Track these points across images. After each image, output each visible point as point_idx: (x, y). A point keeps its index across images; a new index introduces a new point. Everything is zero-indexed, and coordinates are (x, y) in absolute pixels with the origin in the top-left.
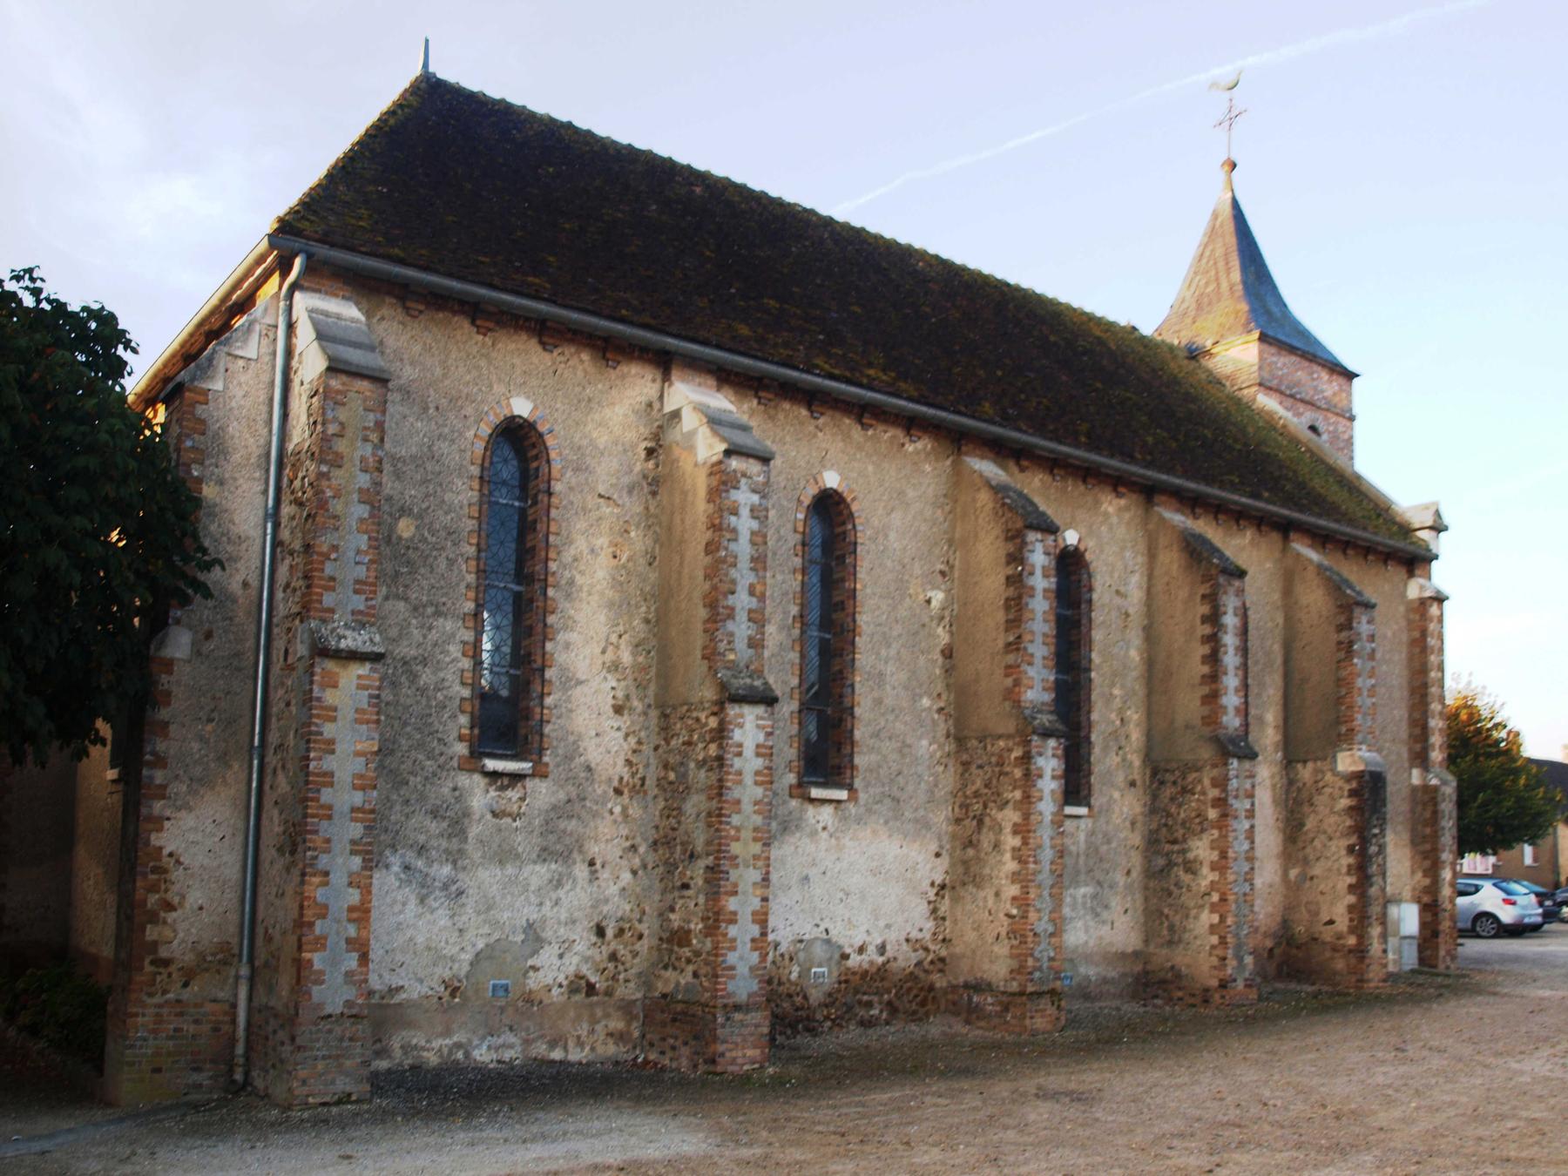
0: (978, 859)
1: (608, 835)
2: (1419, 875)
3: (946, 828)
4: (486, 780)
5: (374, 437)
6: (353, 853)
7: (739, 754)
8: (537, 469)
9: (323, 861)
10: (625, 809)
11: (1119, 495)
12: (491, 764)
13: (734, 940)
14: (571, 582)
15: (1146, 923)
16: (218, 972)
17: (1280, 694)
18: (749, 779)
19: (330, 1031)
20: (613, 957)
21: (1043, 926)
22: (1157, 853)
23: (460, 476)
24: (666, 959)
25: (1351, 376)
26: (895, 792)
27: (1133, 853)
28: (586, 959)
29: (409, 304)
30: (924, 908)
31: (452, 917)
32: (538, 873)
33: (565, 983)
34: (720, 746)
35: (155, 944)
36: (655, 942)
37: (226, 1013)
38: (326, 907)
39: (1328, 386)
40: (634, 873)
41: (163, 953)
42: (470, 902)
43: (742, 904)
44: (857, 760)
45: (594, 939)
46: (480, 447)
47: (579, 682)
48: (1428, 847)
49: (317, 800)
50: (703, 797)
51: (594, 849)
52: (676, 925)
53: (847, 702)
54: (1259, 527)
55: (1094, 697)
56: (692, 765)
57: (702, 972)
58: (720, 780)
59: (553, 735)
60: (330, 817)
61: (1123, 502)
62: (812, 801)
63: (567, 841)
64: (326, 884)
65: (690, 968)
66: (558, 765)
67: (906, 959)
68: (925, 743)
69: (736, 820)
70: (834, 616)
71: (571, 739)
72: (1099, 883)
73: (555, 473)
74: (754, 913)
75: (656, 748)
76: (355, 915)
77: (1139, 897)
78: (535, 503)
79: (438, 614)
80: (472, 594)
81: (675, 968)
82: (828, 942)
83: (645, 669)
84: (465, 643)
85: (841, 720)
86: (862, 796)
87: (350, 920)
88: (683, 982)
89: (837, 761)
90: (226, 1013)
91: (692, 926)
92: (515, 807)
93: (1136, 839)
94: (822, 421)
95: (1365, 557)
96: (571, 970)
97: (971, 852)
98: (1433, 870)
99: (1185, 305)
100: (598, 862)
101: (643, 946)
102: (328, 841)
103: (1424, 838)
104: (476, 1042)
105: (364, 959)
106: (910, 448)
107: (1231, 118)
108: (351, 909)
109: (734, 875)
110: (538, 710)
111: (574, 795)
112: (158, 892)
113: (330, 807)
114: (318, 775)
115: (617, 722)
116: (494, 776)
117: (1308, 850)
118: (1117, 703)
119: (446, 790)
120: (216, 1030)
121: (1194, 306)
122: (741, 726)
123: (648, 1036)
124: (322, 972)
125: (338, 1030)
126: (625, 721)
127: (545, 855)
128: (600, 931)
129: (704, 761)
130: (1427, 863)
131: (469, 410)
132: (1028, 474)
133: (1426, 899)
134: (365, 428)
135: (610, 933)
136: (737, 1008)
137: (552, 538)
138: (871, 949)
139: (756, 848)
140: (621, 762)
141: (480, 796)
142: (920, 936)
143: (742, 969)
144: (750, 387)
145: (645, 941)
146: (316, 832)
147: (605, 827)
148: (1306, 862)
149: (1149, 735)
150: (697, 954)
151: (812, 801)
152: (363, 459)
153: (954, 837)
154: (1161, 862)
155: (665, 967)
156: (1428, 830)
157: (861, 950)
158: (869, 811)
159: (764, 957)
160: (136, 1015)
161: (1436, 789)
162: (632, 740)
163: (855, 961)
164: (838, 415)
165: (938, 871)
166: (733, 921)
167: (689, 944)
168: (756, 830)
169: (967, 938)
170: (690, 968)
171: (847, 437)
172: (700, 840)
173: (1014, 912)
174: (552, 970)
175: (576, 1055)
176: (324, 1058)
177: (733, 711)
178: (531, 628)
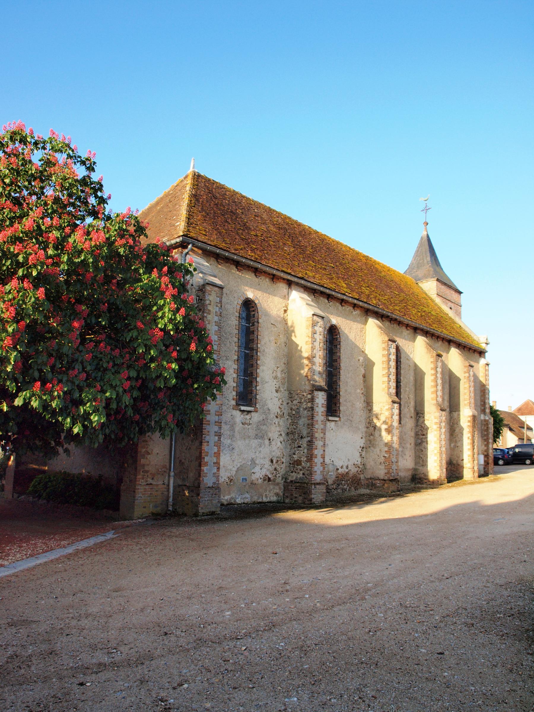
0: (374, 440)
1: (276, 431)
2: (483, 446)
3: (364, 430)
4: (241, 413)
5: (219, 305)
6: (215, 435)
7: (318, 407)
8: (254, 315)
9: (207, 438)
10: (279, 423)
11: (407, 330)
12: (243, 408)
13: (316, 463)
14: (264, 351)
15: (415, 460)
16: (162, 474)
17: (448, 391)
18: (320, 414)
19: (209, 492)
20: (275, 469)
21: (394, 460)
22: (418, 438)
23: (233, 316)
24: (292, 470)
25: (460, 293)
26: (351, 418)
27: (412, 438)
28: (268, 470)
29: (219, 261)
30: (358, 454)
31: (231, 456)
32: (255, 443)
33: (262, 478)
34: (312, 404)
35: (144, 465)
36: (288, 464)
37: (165, 488)
38: (208, 452)
39: (455, 295)
40: (281, 443)
41: (146, 468)
42: (236, 451)
43: (318, 452)
44: (341, 408)
45: (270, 463)
46: (239, 307)
47: (267, 382)
48: (485, 438)
49: (206, 419)
50: (306, 419)
51: (270, 435)
52: (296, 459)
53: (338, 390)
54: (443, 341)
55: (402, 391)
56: (302, 409)
57: (306, 473)
58: (313, 414)
59: (259, 399)
60: (209, 424)
61: (408, 332)
62: (329, 420)
63: (263, 432)
64: (208, 445)
65: (301, 472)
66: (260, 408)
67: (354, 470)
68: (358, 403)
69: (316, 426)
70: (334, 364)
71: (264, 400)
72: (403, 447)
73: (259, 317)
74: (321, 455)
75: (288, 404)
76: (216, 455)
77: (413, 451)
78: (253, 325)
79: (227, 359)
80: (237, 354)
81: (295, 472)
82: (333, 464)
83: (284, 379)
84: (235, 369)
85: (336, 396)
86: (342, 419)
87: (214, 456)
88: (299, 476)
89: (334, 409)
90: (165, 488)
91: (302, 459)
92: (248, 422)
93: (413, 434)
94: (331, 303)
95: (464, 349)
96: (264, 473)
97: (372, 437)
98: (487, 445)
99: (414, 265)
100: (271, 439)
101: (283, 466)
102: (209, 432)
103: (485, 435)
104: (237, 497)
105: (218, 469)
106: (354, 313)
107: (426, 210)
108: (215, 453)
109: (316, 443)
110: (255, 391)
111: (264, 418)
112: (145, 448)
113: (209, 421)
114: (206, 411)
115: (276, 394)
116: (243, 411)
117: (457, 438)
118: (407, 393)
119: (229, 416)
120: (162, 493)
121: (416, 266)
122: (318, 398)
123: (286, 494)
124: (206, 473)
125: (211, 491)
126: (278, 395)
127: (256, 437)
128: (272, 461)
129: (306, 408)
130: (486, 443)
131: (235, 295)
132: (384, 322)
133: (486, 453)
134: (217, 303)
135: (274, 462)
136: (318, 484)
137: (259, 337)
138: (344, 467)
139: (322, 435)
140: (278, 407)
141: (238, 417)
142: (357, 463)
143: (318, 472)
144: (312, 292)
145: (284, 464)
146: (205, 429)
147: (273, 428)
148: (456, 442)
149: (415, 402)
150: (304, 468)
151: (329, 420)
152: (216, 312)
153: (366, 432)
154: (420, 441)
155: (292, 472)
156: (486, 433)
157: (342, 467)
158: (344, 424)
159: (324, 468)
160: (139, 489)
161: (488, 421)
162: (281, 401)
163: (340, 471)
164: (335, 302)
165: (361, 443)
166: (316, 457)
167: (301, 464)
168: (322, 429)
169: (370, 464)
170: (301, 472)
171: (338, 309)
172: (305, 433)
173: (386, 455)
174: (258, 474)
175: (265, 500)
176: (208, 500)
177: (316, 393)
178: (252, 365)
